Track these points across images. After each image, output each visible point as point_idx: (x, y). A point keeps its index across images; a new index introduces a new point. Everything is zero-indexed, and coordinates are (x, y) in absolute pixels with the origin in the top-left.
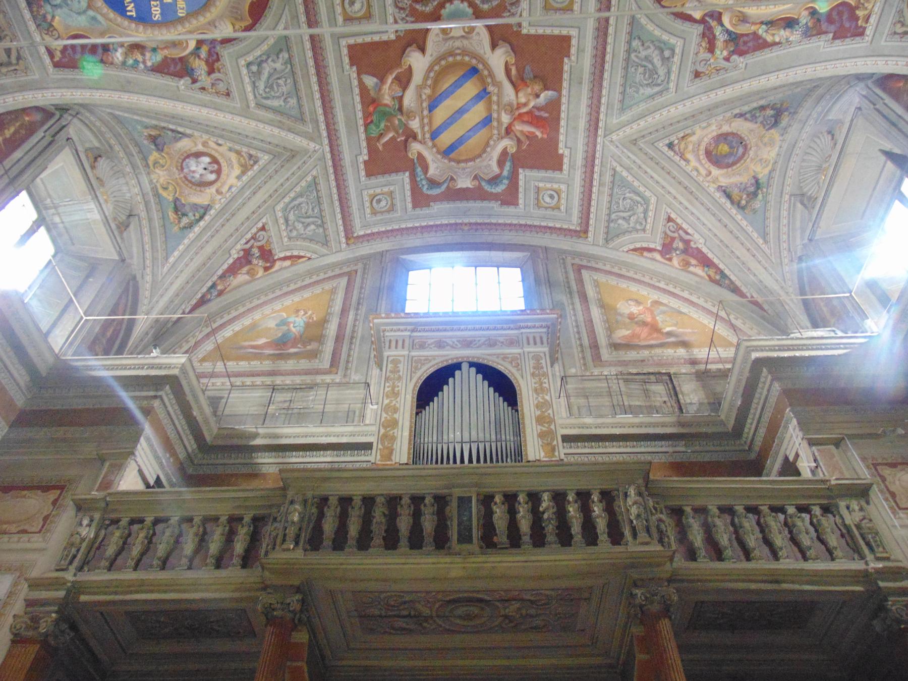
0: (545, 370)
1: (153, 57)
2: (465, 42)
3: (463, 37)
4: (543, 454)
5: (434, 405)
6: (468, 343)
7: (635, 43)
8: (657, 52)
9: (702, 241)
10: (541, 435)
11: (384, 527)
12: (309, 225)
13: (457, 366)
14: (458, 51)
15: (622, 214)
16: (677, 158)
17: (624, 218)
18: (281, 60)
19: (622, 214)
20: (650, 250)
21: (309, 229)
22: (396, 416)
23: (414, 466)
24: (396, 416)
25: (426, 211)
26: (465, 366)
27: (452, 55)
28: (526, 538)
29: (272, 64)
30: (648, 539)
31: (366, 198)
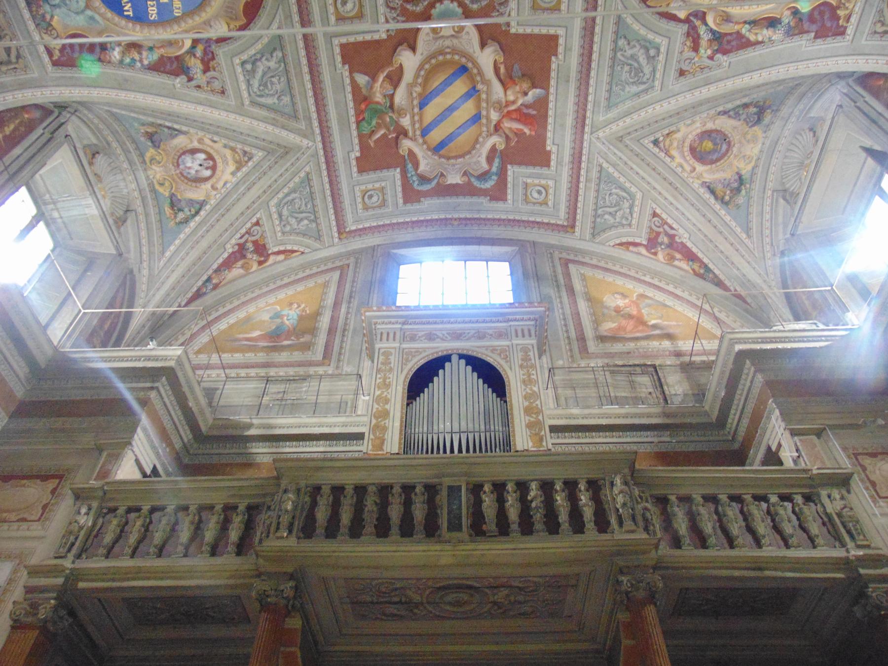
0: (533, 361)
1: (150, 56)
2: (455, 41)
3: (452, 36)
4: (531, 444)
5: (425, 396)
6: (457, 336)
7: (621, 42)
8: (642, 51)
9: (686, 235)
10: (529, 426)
11: (375, 516)
12: (302, 220)
13: (447, 358)
14: (448, 50)
15: (608, 210)
16: (662, 155)
17: (610, 213)
18: (274, 59)
19: (608, 210)
20: (636, 245)
21: (302, 224)
22: (387, 407)
23: (405, 456)
24: (387, 407)
25: (416, 206)
26: (455, 358)
27: (442, 54)
28: (515, 527)
29: (266, 62)
30: (634, 528)
31: (358, 194)
